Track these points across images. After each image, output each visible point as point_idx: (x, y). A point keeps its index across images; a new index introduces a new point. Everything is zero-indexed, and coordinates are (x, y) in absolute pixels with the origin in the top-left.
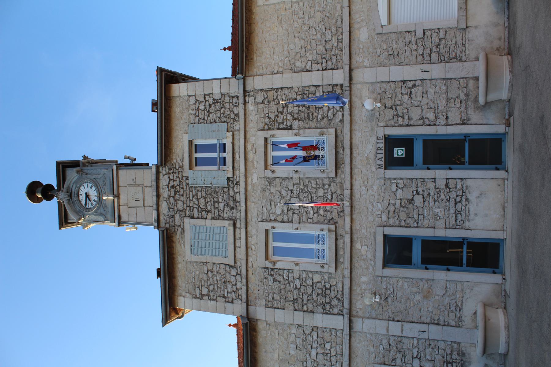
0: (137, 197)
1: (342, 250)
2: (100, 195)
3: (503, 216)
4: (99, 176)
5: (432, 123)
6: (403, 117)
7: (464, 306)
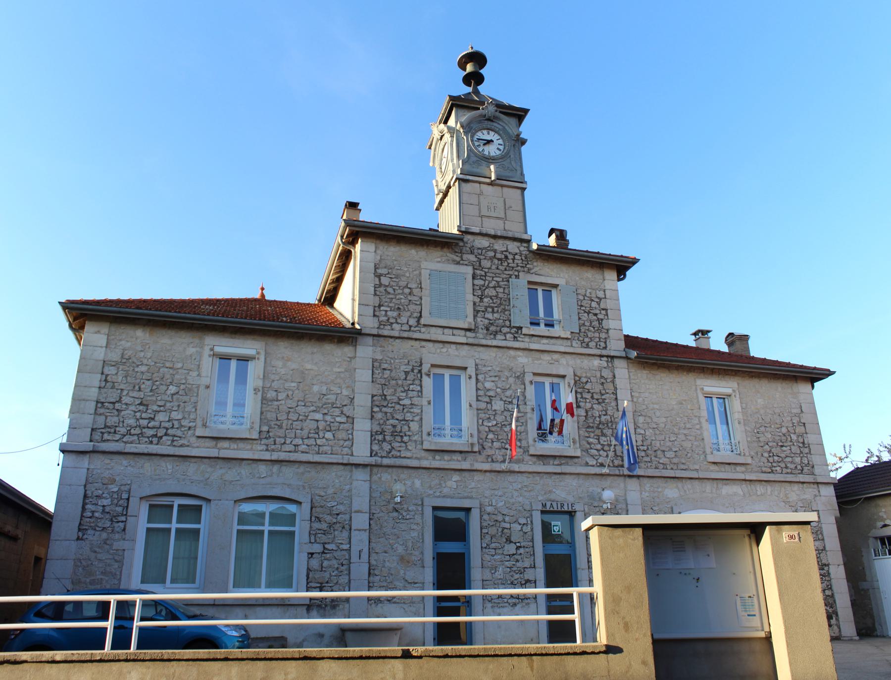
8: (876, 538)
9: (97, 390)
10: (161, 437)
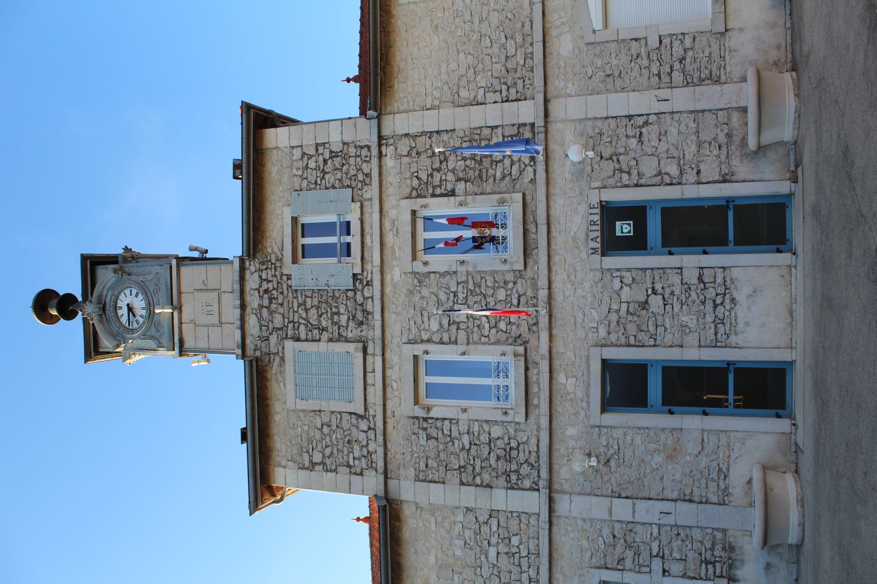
0: (210, 308)
1: (535, 386)
2: (150, 307)
3: (791, 325)
5: (674, 181)
6: (629, 173)
7: (731, 470)
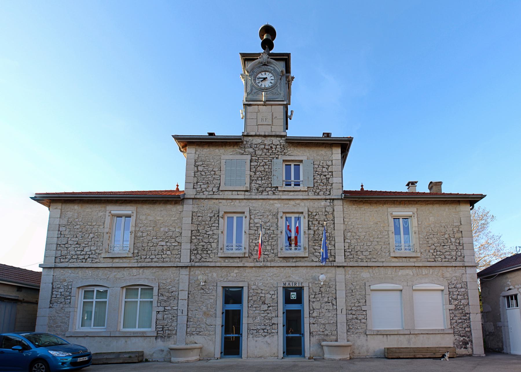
0: (264, 120)
2: (265, 89)
3: (256, 357)
4: (279, 90)
6: (314, 298)
8: (504, 296)
9: (56, 239)
10: (87, 259)
